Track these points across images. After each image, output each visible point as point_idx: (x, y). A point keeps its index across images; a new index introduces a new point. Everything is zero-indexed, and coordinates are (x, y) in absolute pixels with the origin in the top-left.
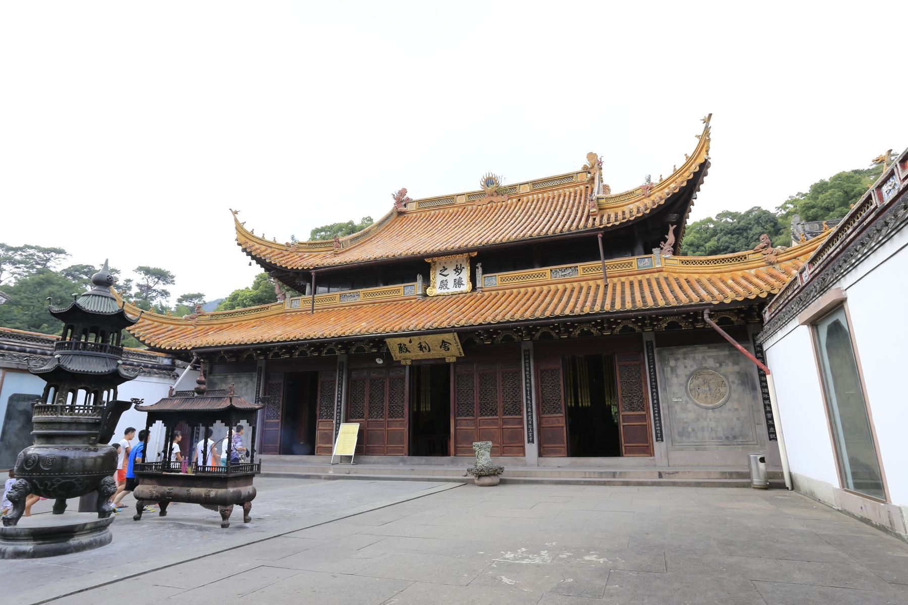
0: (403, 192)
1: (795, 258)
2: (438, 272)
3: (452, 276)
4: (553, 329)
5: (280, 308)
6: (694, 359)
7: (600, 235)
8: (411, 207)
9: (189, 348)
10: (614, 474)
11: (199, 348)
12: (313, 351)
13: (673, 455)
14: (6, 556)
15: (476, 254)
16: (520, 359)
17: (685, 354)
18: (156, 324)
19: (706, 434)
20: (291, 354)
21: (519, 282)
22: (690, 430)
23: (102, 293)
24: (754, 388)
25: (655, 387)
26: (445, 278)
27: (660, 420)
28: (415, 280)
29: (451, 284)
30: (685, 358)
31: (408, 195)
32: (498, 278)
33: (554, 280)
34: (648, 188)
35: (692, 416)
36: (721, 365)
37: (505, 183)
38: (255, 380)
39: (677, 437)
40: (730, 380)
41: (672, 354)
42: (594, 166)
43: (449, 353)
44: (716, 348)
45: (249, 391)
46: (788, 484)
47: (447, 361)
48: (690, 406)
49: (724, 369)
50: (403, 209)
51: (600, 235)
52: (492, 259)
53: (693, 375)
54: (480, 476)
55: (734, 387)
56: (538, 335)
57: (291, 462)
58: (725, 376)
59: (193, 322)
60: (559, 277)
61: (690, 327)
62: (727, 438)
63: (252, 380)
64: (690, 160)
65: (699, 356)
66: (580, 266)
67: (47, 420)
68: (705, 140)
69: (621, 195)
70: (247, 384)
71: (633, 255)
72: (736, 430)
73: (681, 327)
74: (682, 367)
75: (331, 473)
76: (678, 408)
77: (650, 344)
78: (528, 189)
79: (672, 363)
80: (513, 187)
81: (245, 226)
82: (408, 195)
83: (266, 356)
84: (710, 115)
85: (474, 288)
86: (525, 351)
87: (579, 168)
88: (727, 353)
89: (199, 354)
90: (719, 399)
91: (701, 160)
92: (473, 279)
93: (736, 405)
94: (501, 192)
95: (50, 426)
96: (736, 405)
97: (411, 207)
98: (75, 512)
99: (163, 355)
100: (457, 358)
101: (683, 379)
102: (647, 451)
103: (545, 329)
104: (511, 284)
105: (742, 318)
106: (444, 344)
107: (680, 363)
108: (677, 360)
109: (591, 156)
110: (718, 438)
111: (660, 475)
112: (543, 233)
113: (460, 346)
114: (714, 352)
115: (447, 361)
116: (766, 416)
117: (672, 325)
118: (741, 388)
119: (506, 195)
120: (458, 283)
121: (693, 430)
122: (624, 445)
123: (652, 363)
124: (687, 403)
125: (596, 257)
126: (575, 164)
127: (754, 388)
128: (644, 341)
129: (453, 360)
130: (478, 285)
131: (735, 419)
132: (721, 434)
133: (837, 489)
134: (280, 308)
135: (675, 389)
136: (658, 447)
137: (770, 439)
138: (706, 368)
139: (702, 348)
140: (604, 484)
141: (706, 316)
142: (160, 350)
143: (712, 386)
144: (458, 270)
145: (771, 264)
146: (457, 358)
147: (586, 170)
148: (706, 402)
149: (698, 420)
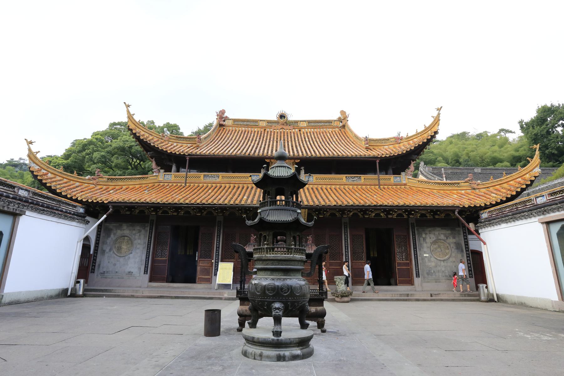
0: (223, 112)
1: (488, 188)
5: (156, 179)
6: (434, 234)
7: (378, 161)
9: (105, 202)
10: (408, 295)
11: (115, 202)
14: (287, 359)
16: (341, 227)
17: (430, 231)
18: (65, 180)
19: (440, 274)
20: (178, 212)
21: (327, 181)
24: (462, 251)
25: (415, 248)
27: (418, 266)
31: (226, 115)
32: (314, 177)
33: (347, 183)
34: (398, 140)
35: (433, 264)
37: (291, 118)
39: (426, 275)
41: (424, 231)
42: (221, 116)
44: (445, 229)
45: (142, 237)
46: (496, 299)
48: (433, 259)
50: (222, 123)
53: (434, 242)
54: (342, 296)
55: (453, 250)
56: (351, 214)
57: (178, 288)
58: (449, 244)
59: (94, 182)
64: (427, 129)
65: (437, 233)
66: (363, 177)
67: (287, 258)
68: (437, 121)
69: (376, 140)
70: (140, 231)
71: (386, 174)
75: (226, 296)
76: (426, 260)
77: (413, 225)
78: (305, 125)
79: (424, 236)
80: (296, 122)
81: (134, 117)
82: (226, 115)
83: (157, 212)
86: (344, 223)
87: (335, 118)
88: (450, 232)
89: (114, 207)
90: (446, 256)
91: (434, 130)
93: (454, 259)
94: (288, 123)
95: (288, 263)
96: (454, 259)
98: (291, 327)
99: (80, 205)
101: (429, 245)
102: (410, 282)
103: (356, 211)
104: (322, 182)
107: (427, 236)
108: (426, 234)
109: (343, 112)
110: (446, 276)
111: (431, 296)
114: (444, 231)
118: (456, 251)
119: (292, 126)
122: (199, 276)
123: (414, 235)
124: (431, 257)
125: (375, 172)
126: (334, 116)
127: (462, 251)
128: (410, 222)
132: (447, 274)
133: (555, 302)
134: (156, 179)
136: (417, 281)
138: (440, 240)
139: (438, 229)
140: (406, 300)
141: (456, 213)
142: (76, 200)
143: (442, 249)
145: (474, 189)
147: (340, 120)
148: (440, 257)
149: (436, 267)
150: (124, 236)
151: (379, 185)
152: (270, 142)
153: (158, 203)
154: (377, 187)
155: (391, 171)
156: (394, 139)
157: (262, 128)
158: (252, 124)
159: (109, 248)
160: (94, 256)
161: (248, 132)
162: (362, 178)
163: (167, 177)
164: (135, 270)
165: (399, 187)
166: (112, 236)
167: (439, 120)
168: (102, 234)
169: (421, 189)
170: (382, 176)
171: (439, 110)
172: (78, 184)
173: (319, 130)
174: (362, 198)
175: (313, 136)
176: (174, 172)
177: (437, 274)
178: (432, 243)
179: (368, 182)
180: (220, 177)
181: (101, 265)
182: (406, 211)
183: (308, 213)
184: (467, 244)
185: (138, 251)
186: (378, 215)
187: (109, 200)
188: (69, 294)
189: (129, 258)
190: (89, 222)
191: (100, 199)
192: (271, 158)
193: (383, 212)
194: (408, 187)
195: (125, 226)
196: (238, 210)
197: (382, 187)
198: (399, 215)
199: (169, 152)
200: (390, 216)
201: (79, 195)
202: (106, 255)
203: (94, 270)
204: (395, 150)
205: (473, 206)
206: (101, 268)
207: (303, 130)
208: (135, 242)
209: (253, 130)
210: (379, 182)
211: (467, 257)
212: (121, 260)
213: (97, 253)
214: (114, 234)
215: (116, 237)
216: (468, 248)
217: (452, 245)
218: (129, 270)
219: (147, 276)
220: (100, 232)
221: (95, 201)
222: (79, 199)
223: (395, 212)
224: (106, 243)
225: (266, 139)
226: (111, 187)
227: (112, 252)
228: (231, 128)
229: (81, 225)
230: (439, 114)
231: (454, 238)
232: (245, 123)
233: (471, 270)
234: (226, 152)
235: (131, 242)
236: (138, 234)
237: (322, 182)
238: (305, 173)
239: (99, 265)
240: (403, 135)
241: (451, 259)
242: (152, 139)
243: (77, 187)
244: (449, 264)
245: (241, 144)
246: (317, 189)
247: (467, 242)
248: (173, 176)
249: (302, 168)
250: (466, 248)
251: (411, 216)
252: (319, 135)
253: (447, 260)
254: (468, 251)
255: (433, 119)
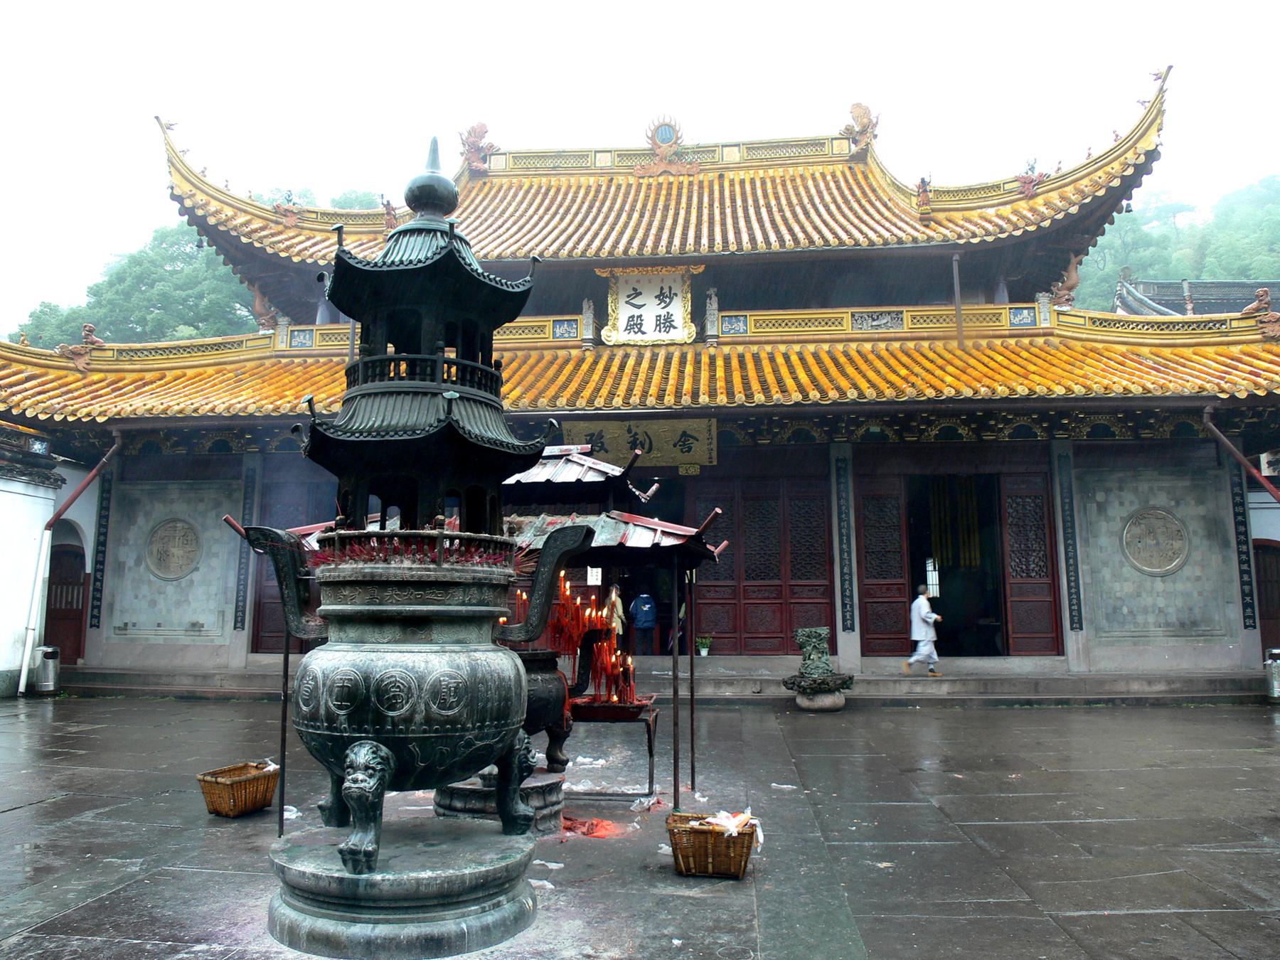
0: (480, 132)
2: (623, 299)
3: (651, 310)
4: (1038, 422)
6: (1135, 491)
7: (956, 257)
8: (496, 163)
9: (100, 420)
12: (176, 444)
13: (1099, 652)
15: (701, 269)
16: (828, 477)
17: (1121, 480)
19: (1151, 619)
22: (1125, 610)
23: (433, 226)
24: (1225, 544)
25: (1070, 536)
26: (636, 312)
27: (1078, 593)
28: (579, 311)
29: (649, 324)
30: (1121, 489)
31: (484, 143)
33: (857, 334)
34: (1029, 187)
35: (1128, 588)
36: (1178, 504)
37: (689, 139)
38: (239, 495)
40: (1191, 529)
42: (860, 136)
43: (687, 457)
47: (682, 472)
48: (1127, 571)
49: (1181, 512)
51: (956, 257)
52: (740, 283)
53: (1135, 518)
55: (1196, 541)
56: (787, 434)
60: (867, 329)
61: (974, 438)
62: (1182, 625)
63: (229, 496)
65: (1144, 487)
66: (907, 312)
68: (1154, 115)
71: (990, 300)
72: (1197, 611)
73: (1113, 434)
74: (1116, 504)
76: (1106, 573)
79: (1100, 497)
84: (1170, 67)
85: (701, 337)
88: (1187, 483)
90: (1172, 560)
91: (1145, 145)
92: (698, 316)
93: (1198, 572)
96: (1198, 572)
97: (496, 163)
100: (702, 467)
101: (1117, 525)
105: (973, 430)
106: (685, 441)
109: (860, 111)
110: (1168, 624)
112: (547, 254)
113: (714, 446)
115: (682, 472)
116: (1243, 591)
117: (949, 433)
118: (1206, 543)
120: (666, 323)
121: (1131, 612)
124: (1122, 565)
125: (946, 296)
126: (826, 121)
129: (695, 471)
130: (711, 330)
131: (1195, 594)
135: (1104, 541)
136: (1072, 640)
137: (1246, 627)
138: (1154, 508)
141: (1206, 418)
143: (1161, 539)
144: (664, 297)
146: (702, 467)
147: (849, 135)
148: (1151, 565)
149: (1139, 595)
150: (175, 520)
151: (960, 338)
152: (688, 212)
153: (251, 416)
154: (954, 344)
155: (1003, 293)
156: (1016, 185)
157: (602, 175)
158: (571, 163)
159: (133, 556)
160: (96, 580)
161: (558, 190)
162: (906, 317)
163: (300, 339)
164: (208, 619)
165: (1026, 341)
166: (141, 520)
167: (1161, 112)
168: (114, 517)
169: (1099, 346)
170: (969, 309)
171: (1162, 77)
172: (31, 371)
173: (780, 171)
174: (893, 378)
175: (559, 198)
176: (323, 323)
177: (1140, 619)
178: (1125, 520)
179: (926, 329)
180: (845, 323)
181: (117, 607)
182: (1044, 415)
183: (720, 434)
184: (1242, 522)
185: (214, 562)
186: (949, 433)
187: (110, 414)
188: (22, 688)
189: (192, 582)
190: (64, 481)
191: (85, 411)
192: (611, 263)
193: (964, 423)
194: (1055, 340)
195: (174, 489)
196: (744, 427)
197: (969, 343)
198: (1017, 432)
199: (296, 259)
200: (988, 436)
201: (28, 402)
202: (129, 576)
203: (98, 618)
204: (1014, 218)
205: (1261, 393)
206: (117, 614)
207: (731, 175)
208: (208, 535)
209: (554, 181)
210: (959, 328)
211: (1241, 562)
212: (170, 589)
213: (102, 571)
214: (147, 514)
215: (151, 524)
216: (1246, 534)
217: (1194, 526)
218: (194, 619)
219: (244, 636)
220: (107, 509)
221: (70, 419)
222: (29, 414)
223: (1007, 422)
224: (127, 540)
225: (644, 206)
226: (130, 377)
227: (143, 566)
228: (505, 180)
229: (41, 492)
230: (1162, 90)
231: (1201, 502)
232: (550, 163)
233: (1251, 606)
234: (621, 247)
235: (192, 538)
236: (214, 513)
237: (773, 333)
238: (720, 310)
239: (111, 606)
240: (1046, 167)
241: (1187, 571)
242: (246, 224)
243: (28, 379)
244: (1180, 587)
245: (542, 224)
246: (787, 358)
247: (1244, 514)
248: (317, 335)
249: (712, 291)
250: (1238, 533)
251: (1060, 434)
252: (780, 188)
253: (1173, 572)
254: (1246, 543)
255: (1142, 112)
